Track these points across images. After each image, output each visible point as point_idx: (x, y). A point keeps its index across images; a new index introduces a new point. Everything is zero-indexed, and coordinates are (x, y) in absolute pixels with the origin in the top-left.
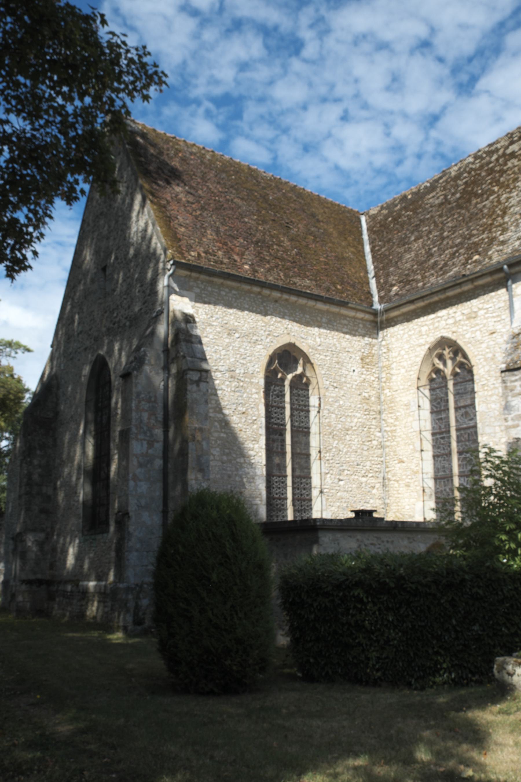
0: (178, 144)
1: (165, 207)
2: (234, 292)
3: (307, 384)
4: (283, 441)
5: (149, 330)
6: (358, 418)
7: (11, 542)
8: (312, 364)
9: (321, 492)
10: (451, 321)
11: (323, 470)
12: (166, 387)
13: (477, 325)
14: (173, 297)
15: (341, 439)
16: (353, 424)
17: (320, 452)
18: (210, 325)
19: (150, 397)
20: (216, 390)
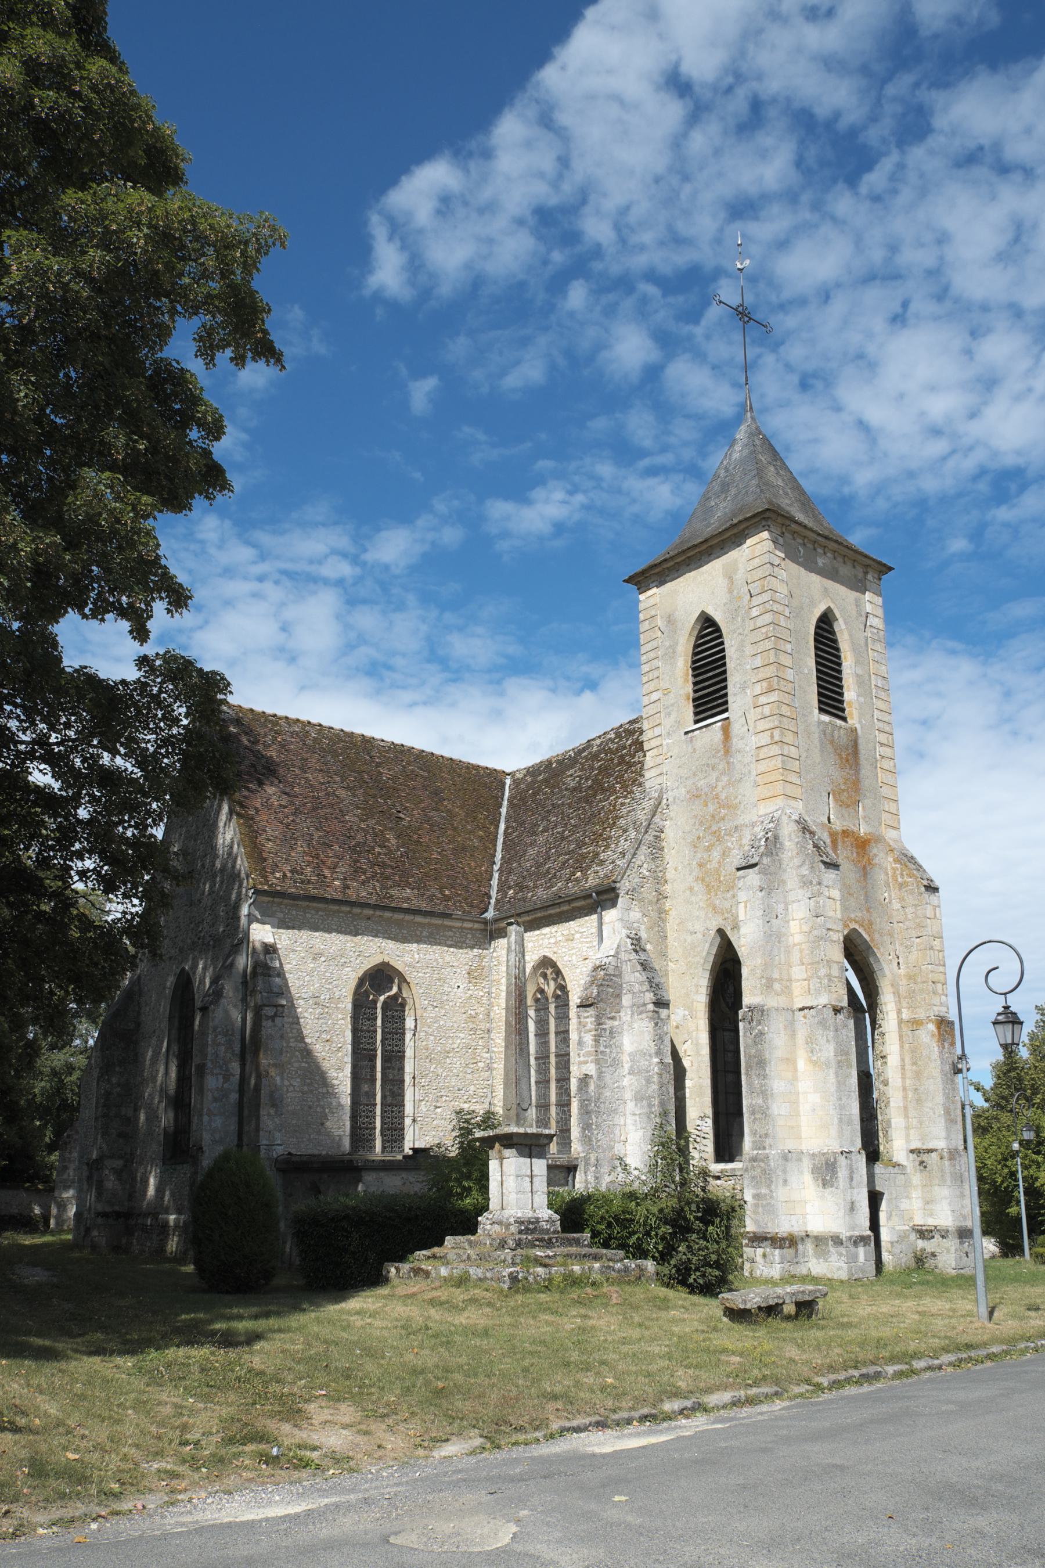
0: (278, 724)
1: (252, 819)
2: (320, 913)
3: (403, 1005)
4: (374, 1067)
5: (229, 961)
6: (462, 1038)
7: (85, 1167)
8: (408, 983)
9: (414, 1121)
10: (552, 940)
11: (417, 1098)
12: (244, 1020)
13: (574, 948)
14: (255, 926)
15: (440, 1063)
16: (455, 1046)
17: (414, 1078)
18: (293, 951)
19: (227, 1031)
20: (298, 1018)
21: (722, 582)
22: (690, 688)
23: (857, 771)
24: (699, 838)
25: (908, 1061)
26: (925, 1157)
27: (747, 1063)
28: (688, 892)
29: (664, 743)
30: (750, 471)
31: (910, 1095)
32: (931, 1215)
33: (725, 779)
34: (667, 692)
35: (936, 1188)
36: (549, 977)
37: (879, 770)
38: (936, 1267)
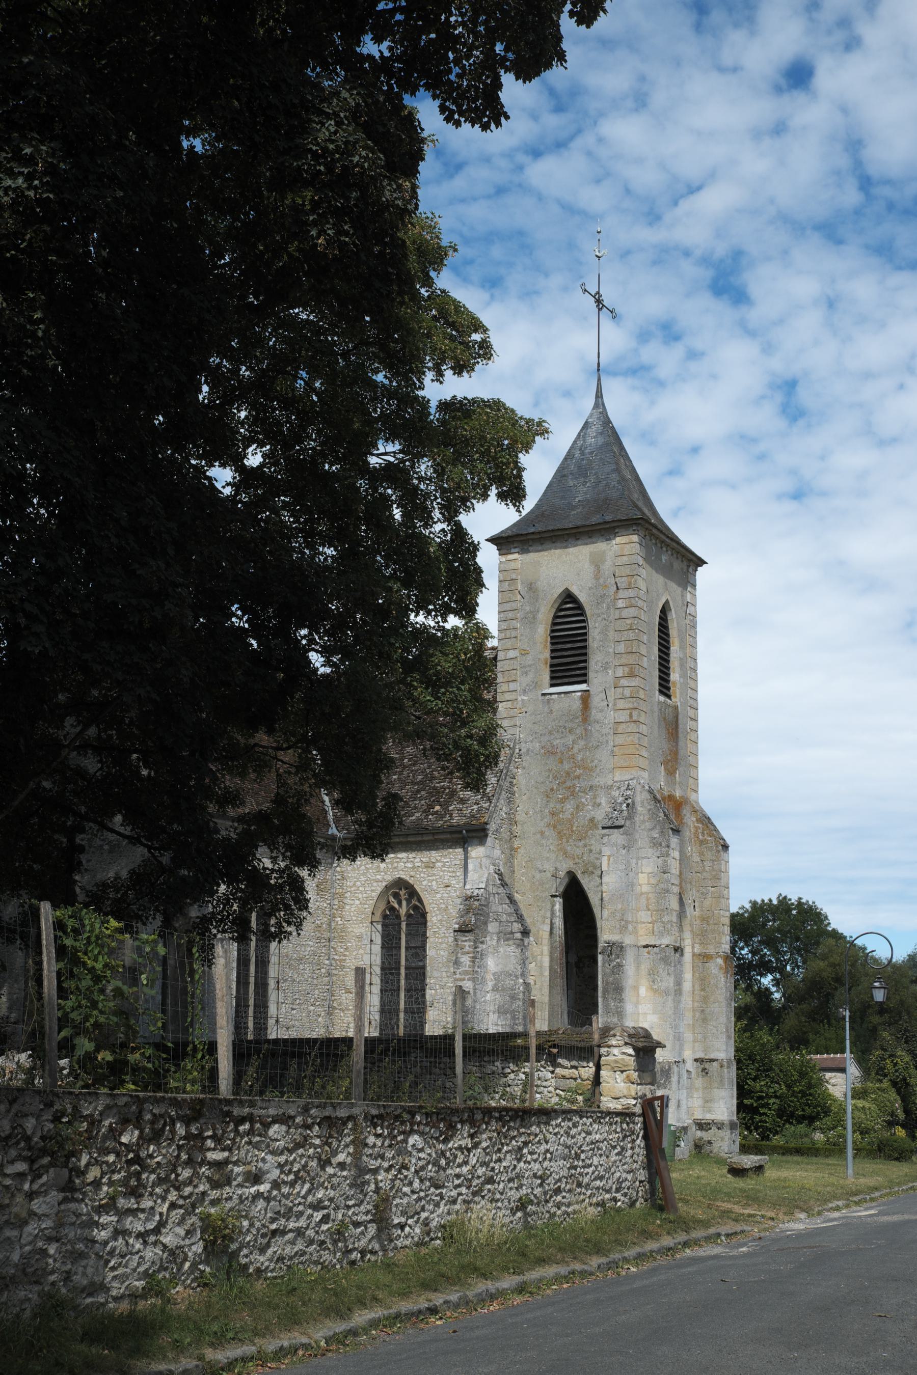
9: (277, 1021)
10: (409, 865)
13: (434, 875)
17: (278, 982)
21: (588, 569)
22: (547, 654)
23: (677, 743)
24: (552, 789)
25: (697, 987)
26: (707, 1065)
27: (604, 988)
28: (539, 836)
29: (520, 698)
30: (609, 463)
31: (698, 1015)
32: (709, 1111)
33: (582, 743)
34: (524, 653)
35: (715, 1090)
36: (403, 897)
37: (689, 741)
38: (711, 1152)
